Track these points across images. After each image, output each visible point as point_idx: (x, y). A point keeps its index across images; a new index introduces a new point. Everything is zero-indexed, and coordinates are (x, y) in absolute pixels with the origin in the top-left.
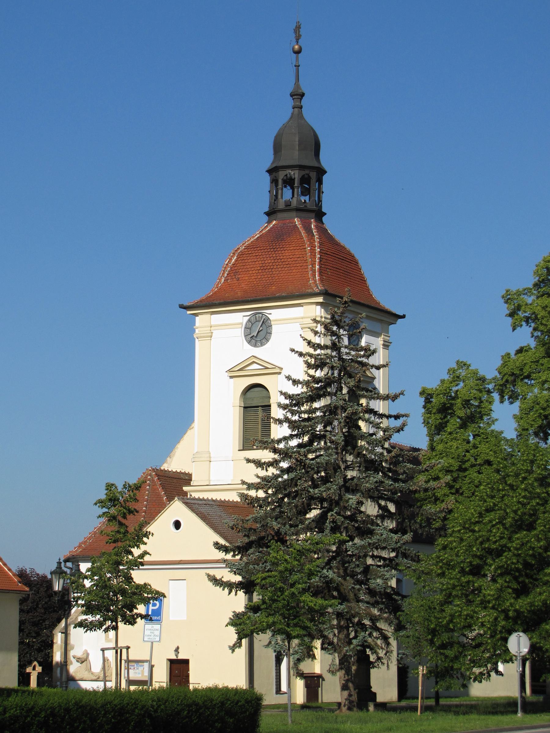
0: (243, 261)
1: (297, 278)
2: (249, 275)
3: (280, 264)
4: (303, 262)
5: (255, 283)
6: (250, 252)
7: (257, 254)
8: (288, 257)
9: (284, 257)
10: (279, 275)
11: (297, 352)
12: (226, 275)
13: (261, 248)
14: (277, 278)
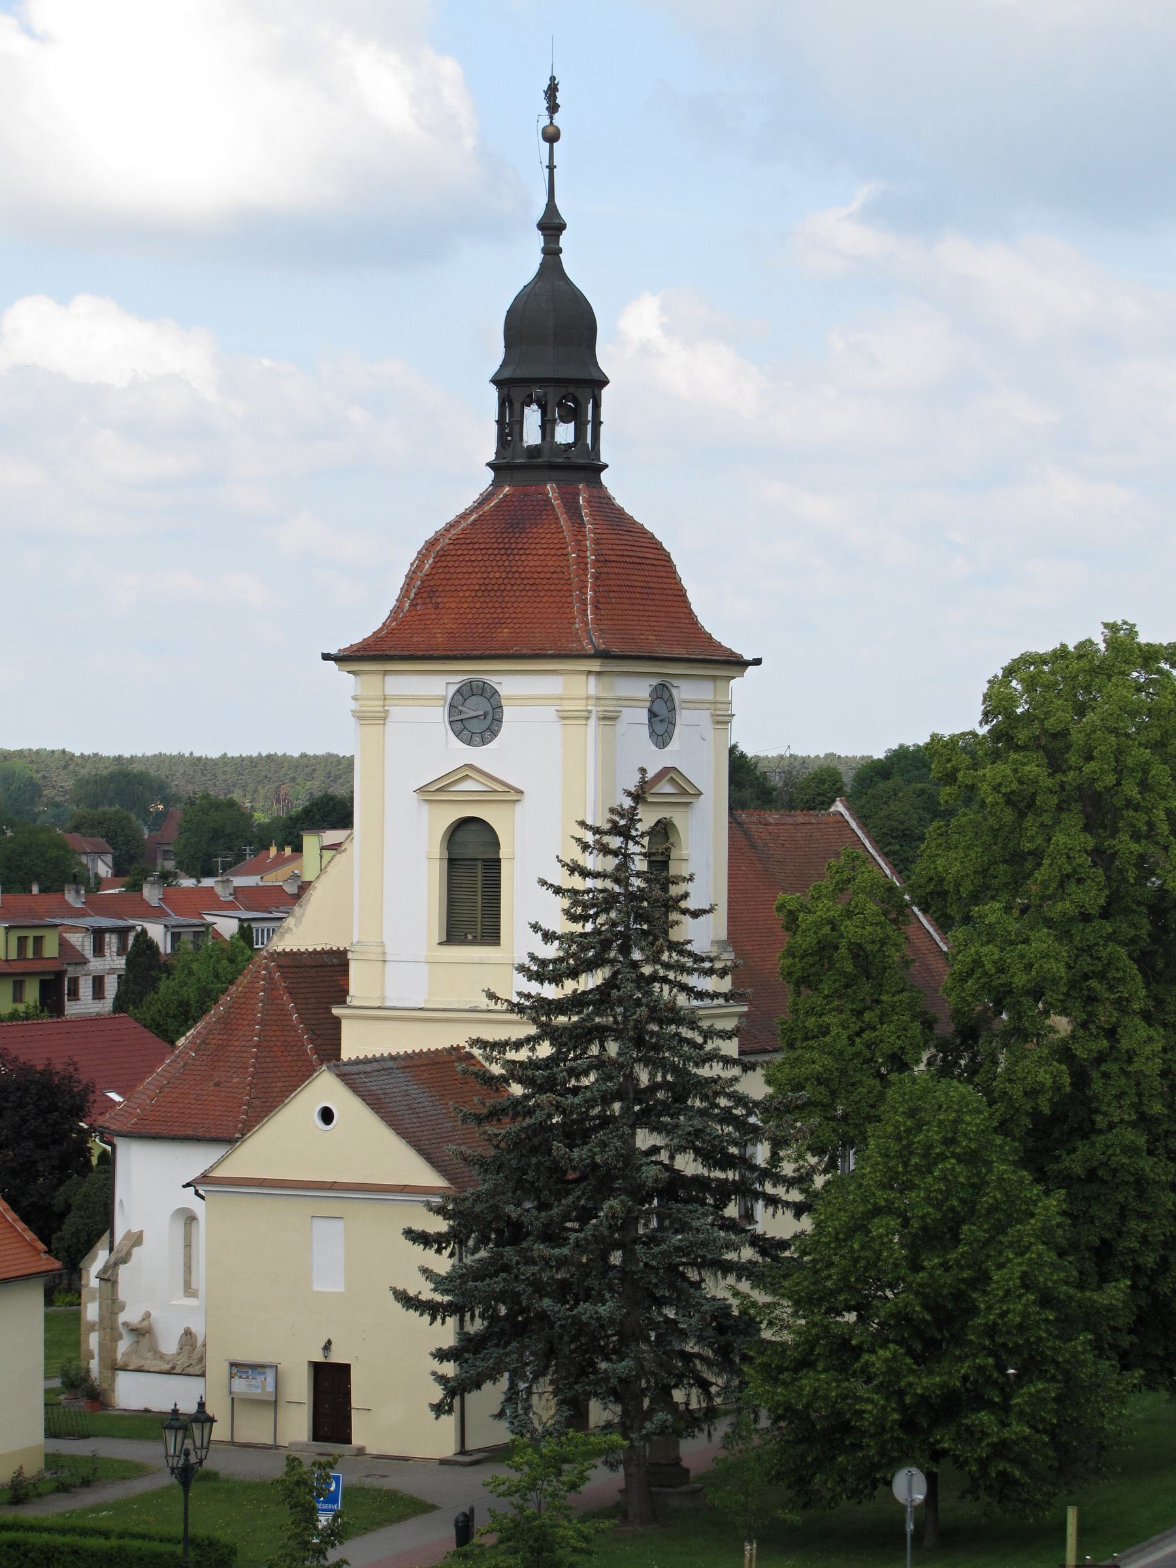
0: (446, 570)
1: (551, 616)
2: (457, 600)
3: (519, 581)
4: (563, 582)
5: (470, 616)
6: (459, 552)
7: (473, 558)
8: (533, 570)
9: (527, 569)
10: (516, 605)
11: (551, 885)
12: (412, 595)
13: (482, 546)
14: (511, 610)
